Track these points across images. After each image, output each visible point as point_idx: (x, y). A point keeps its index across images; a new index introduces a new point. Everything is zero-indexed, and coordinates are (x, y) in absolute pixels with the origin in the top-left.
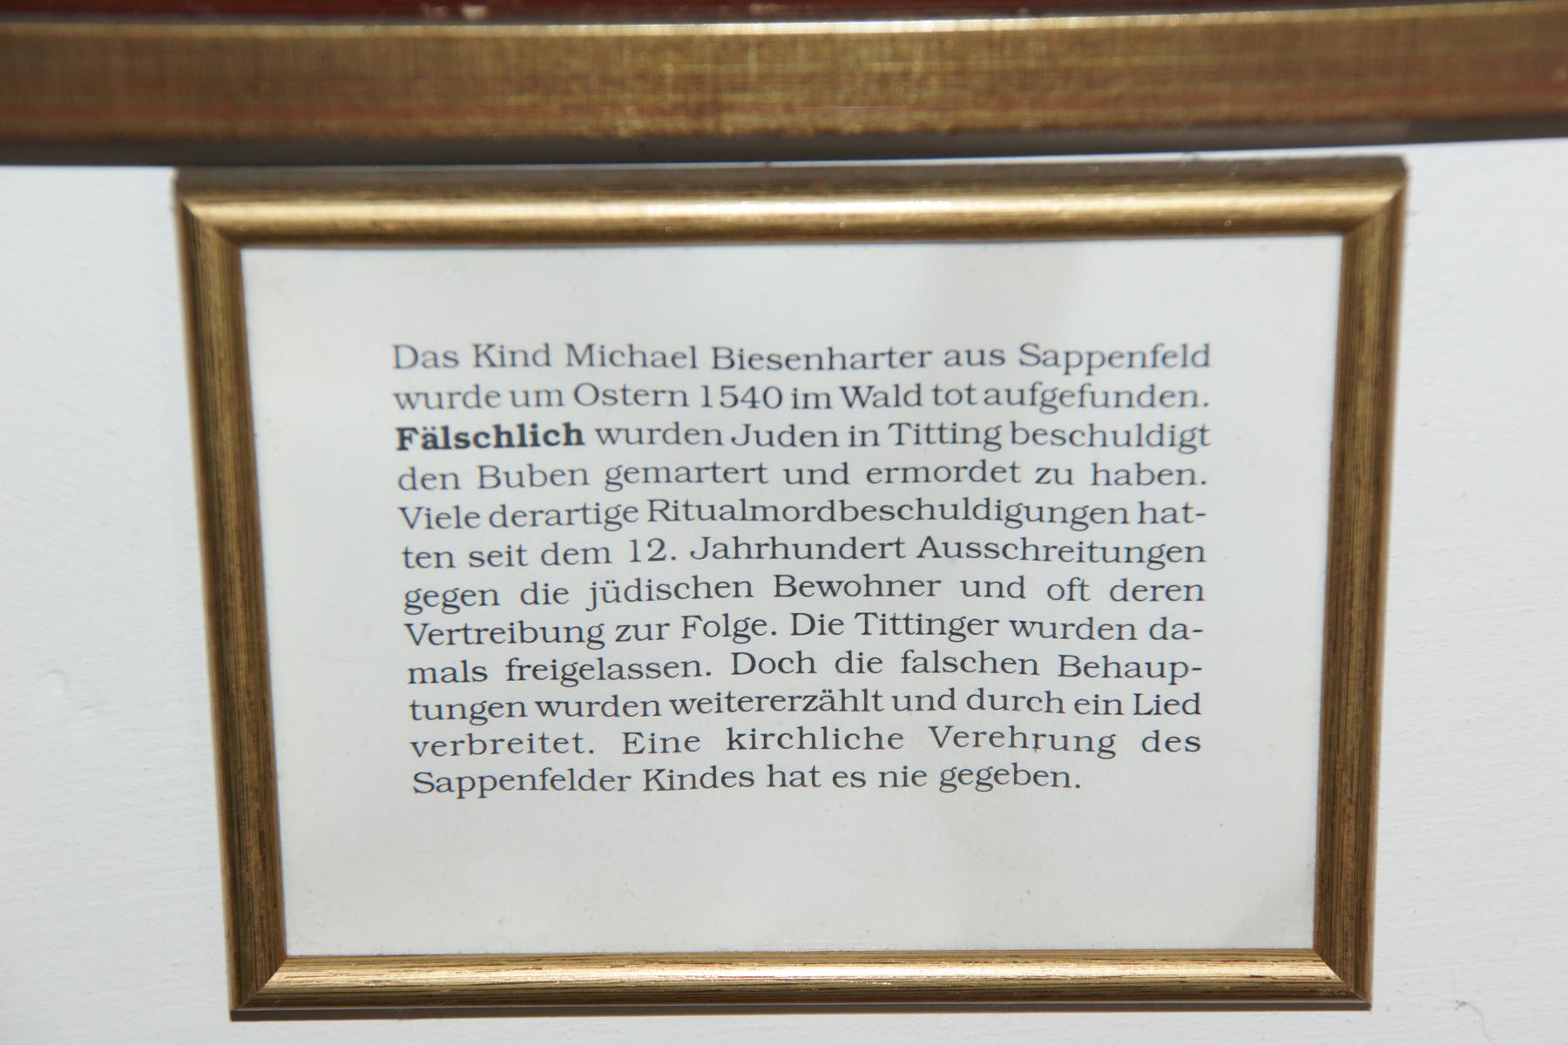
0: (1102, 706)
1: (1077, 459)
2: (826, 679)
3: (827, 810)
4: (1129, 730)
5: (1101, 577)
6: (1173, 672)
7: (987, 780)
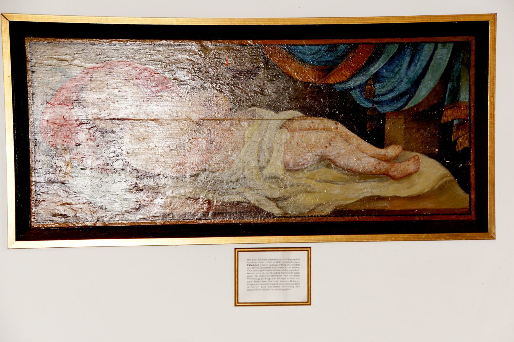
0: (293, 284)
1: (291, 266)
2: (275, 282)
4: (295, 286)
5: (293, 275)
6: (298, 281)
7: (285, 290)
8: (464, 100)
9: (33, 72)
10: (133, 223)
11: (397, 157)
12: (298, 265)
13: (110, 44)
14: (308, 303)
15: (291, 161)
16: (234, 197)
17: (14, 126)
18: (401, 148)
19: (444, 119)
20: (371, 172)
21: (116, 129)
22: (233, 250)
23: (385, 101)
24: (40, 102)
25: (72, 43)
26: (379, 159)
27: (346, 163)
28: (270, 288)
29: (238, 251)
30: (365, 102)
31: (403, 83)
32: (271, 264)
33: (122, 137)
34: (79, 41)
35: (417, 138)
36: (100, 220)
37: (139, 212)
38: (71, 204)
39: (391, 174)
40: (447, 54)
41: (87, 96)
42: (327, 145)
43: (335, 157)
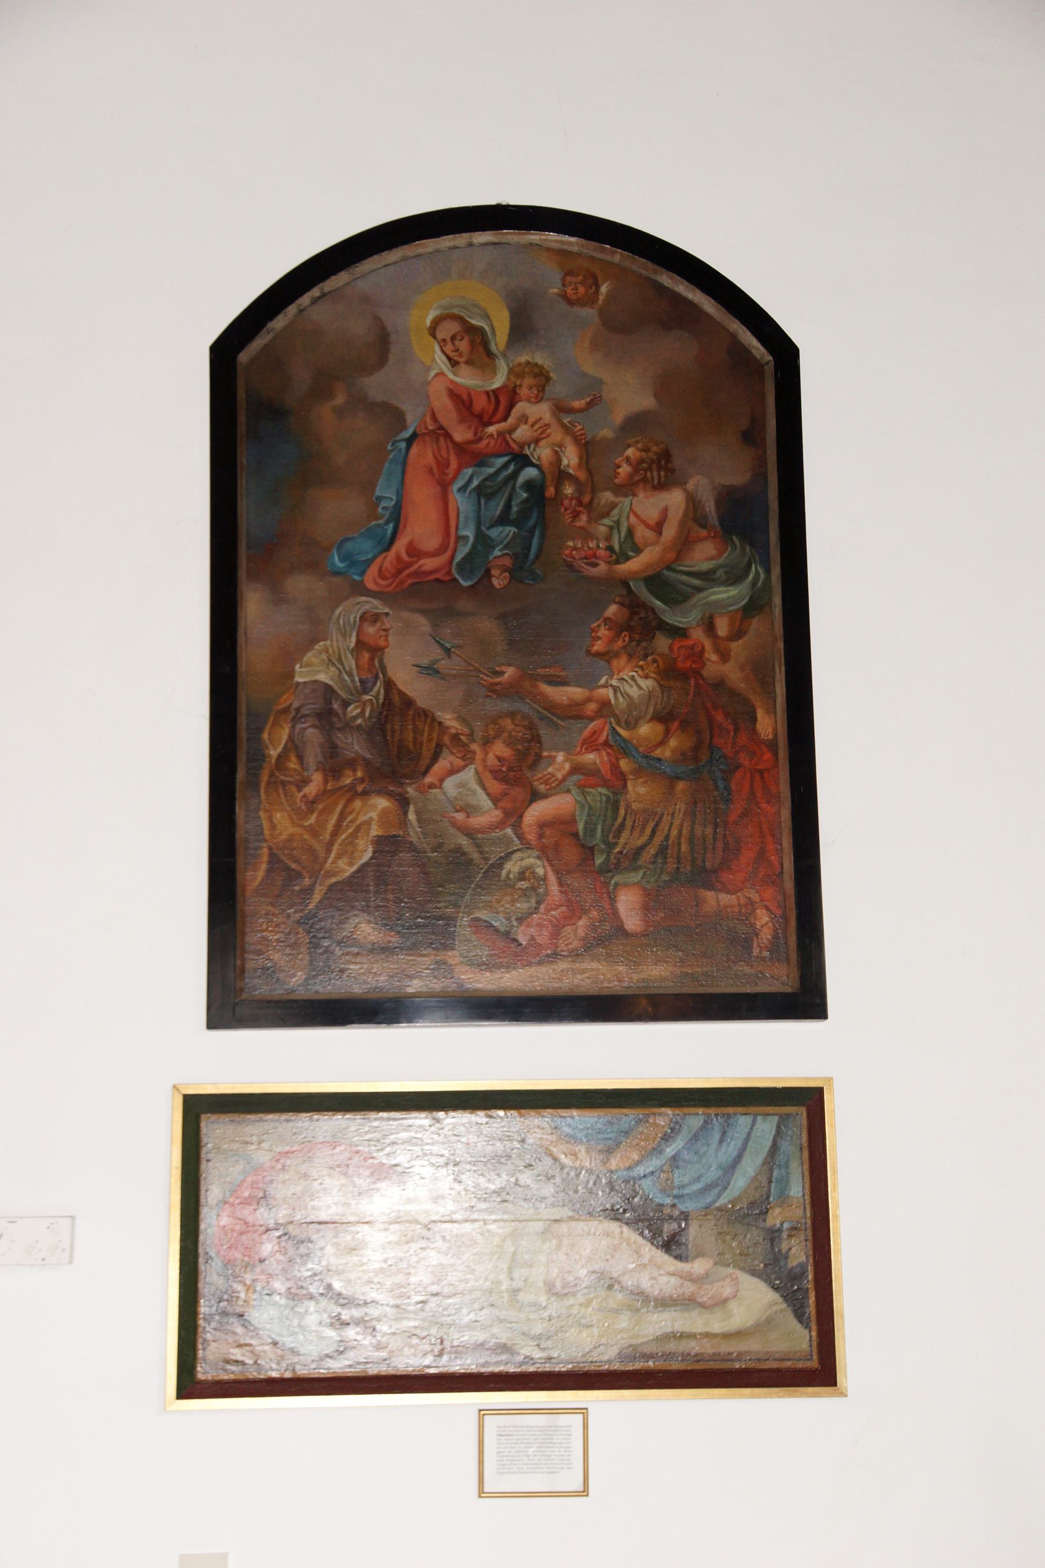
0: (562, 1464)
1: (560, 1437)
2: (536, 1462)
3: (43, 1260)
4: (565, 1466)
5: (562, 1449)
6: (569, 1460)
7: (552, 1473)
8: (796, 1195)
9: (208, 1161)
10: (335, 1373)
11: (707, 1275)
12: (570, 1435)
13: (311, 1119)
14: (585, 1492)
15: (558, 1280)
16: (478, 1333)
17: (181, 1235)
18: (711, 1262)
19: (769, 1222)
20: (671, 1297)
21: (314, 1237)
22: (477, 1412)
23: (687, 1195)
24: (215, 1202)
25: (261, 1120)
26: (681, 1277)
27: (635, 1283)
28: (529, 1470)
29: (484, 1415)
30: (660, 1196)
31: (712, 1169)
32: (532, 1433)
33: (322, 1249)
34: (271, 1116)
35: (733, 1248)
36: (290, 1368)
37: (342, 1356)
38: (250, 1345)
39: (699, 1300)
40: (771, 1130)
41: (279, 1191)
42: (608, 1257)
43: (619, 1275)
